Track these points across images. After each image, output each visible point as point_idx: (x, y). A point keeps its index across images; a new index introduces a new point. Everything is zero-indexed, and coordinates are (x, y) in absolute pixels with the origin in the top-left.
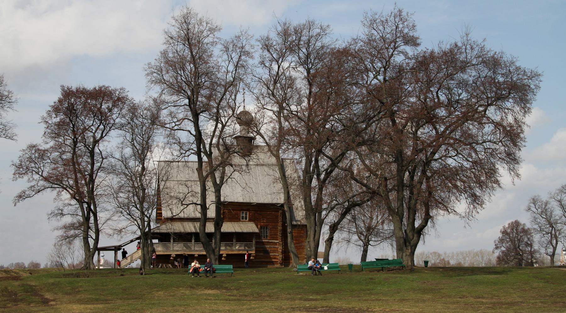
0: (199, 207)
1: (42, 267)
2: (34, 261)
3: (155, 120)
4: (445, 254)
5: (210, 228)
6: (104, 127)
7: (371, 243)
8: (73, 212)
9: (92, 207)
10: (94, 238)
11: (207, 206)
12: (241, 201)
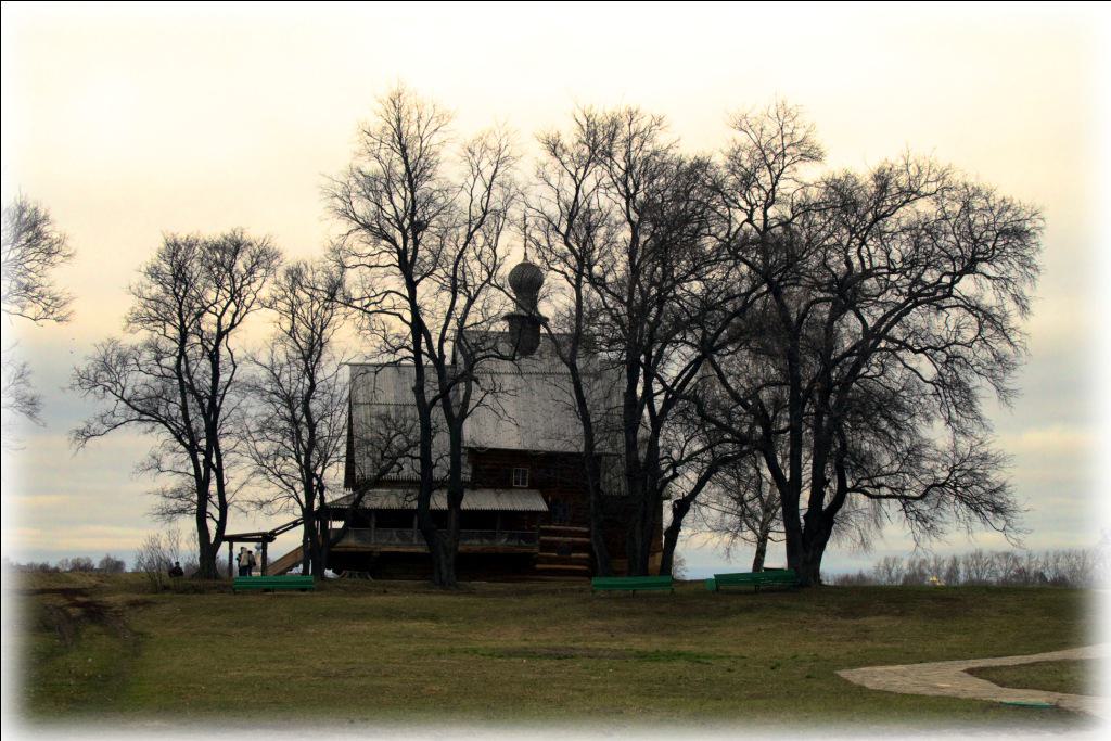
0: (418, 462)
1: (129, 567)
2: (112, 557)
3: (334, 292)
4: (1030, 556)
5: (439, 501)
6: (238, 306)
7: (770, 535)
8: (178, 471)
9: (214, 460)
10: (218, 519)
11: (433, 461)
12: (514, 446)
